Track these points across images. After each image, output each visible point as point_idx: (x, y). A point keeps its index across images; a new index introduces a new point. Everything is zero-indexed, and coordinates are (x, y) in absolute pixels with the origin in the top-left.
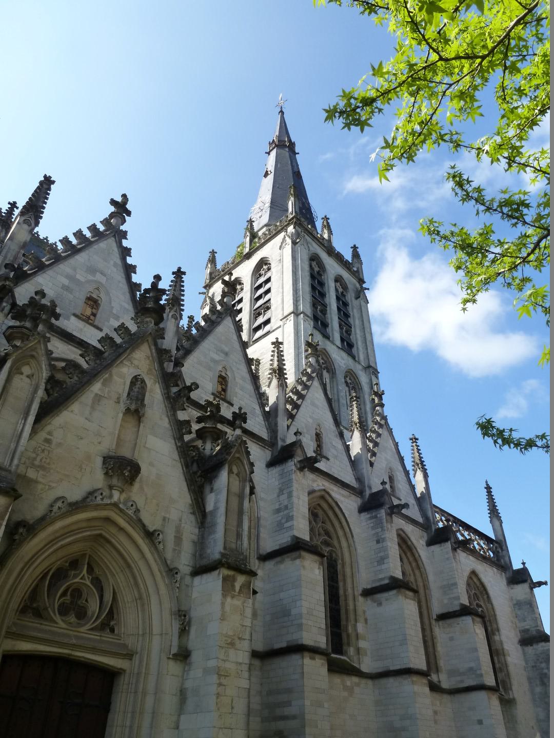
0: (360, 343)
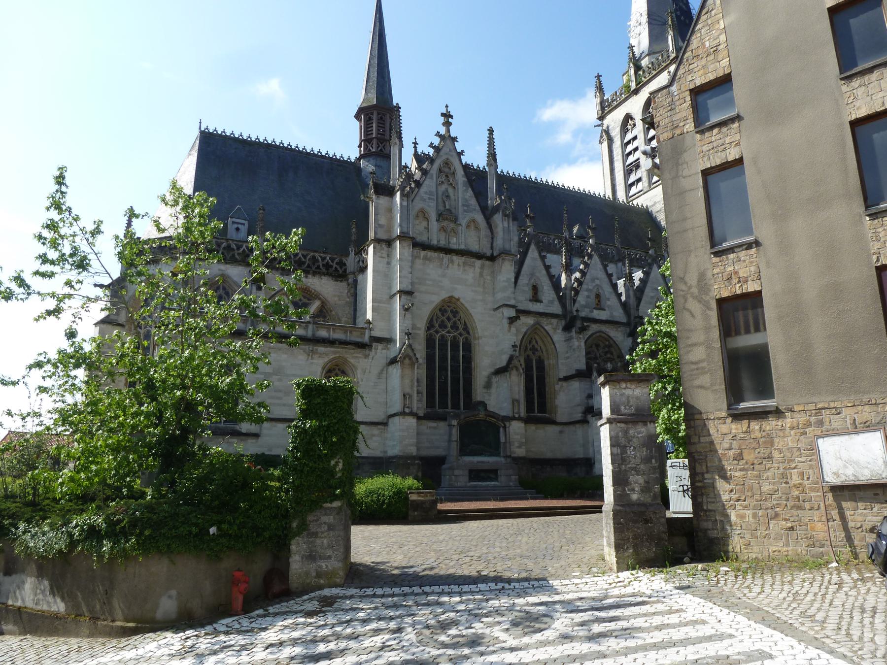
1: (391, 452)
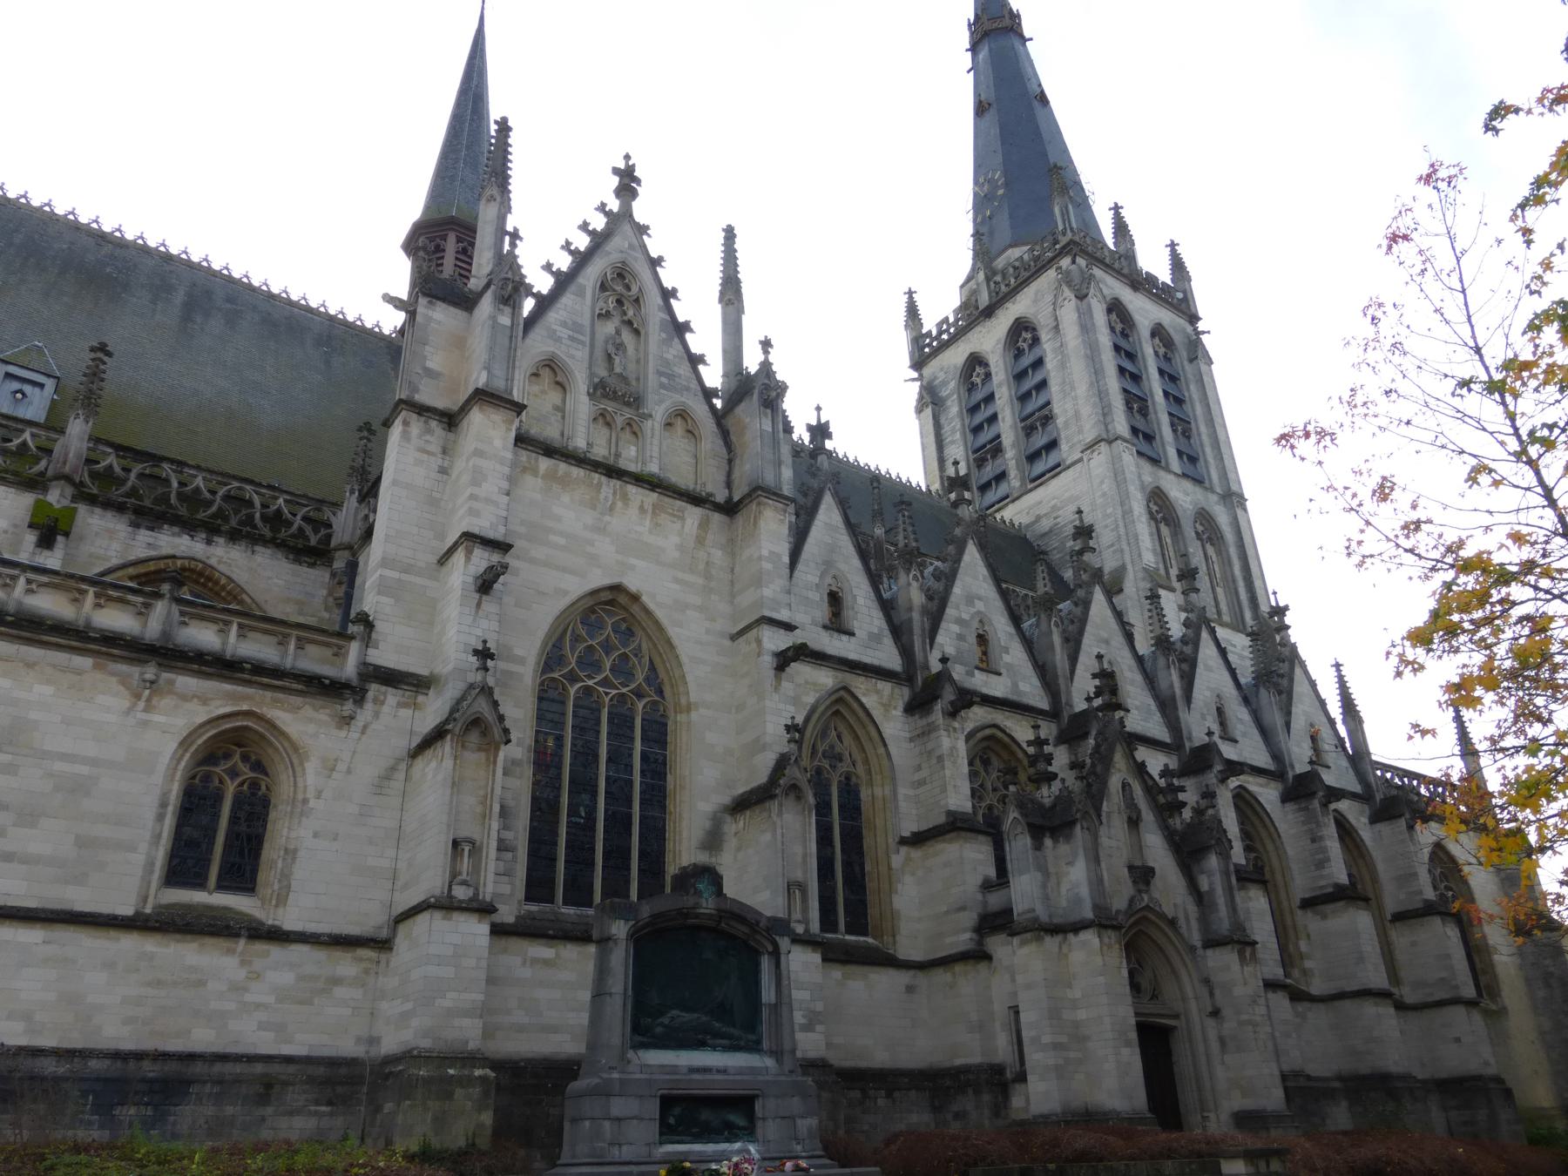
0: (1208, 450)
1: (391, 1042)
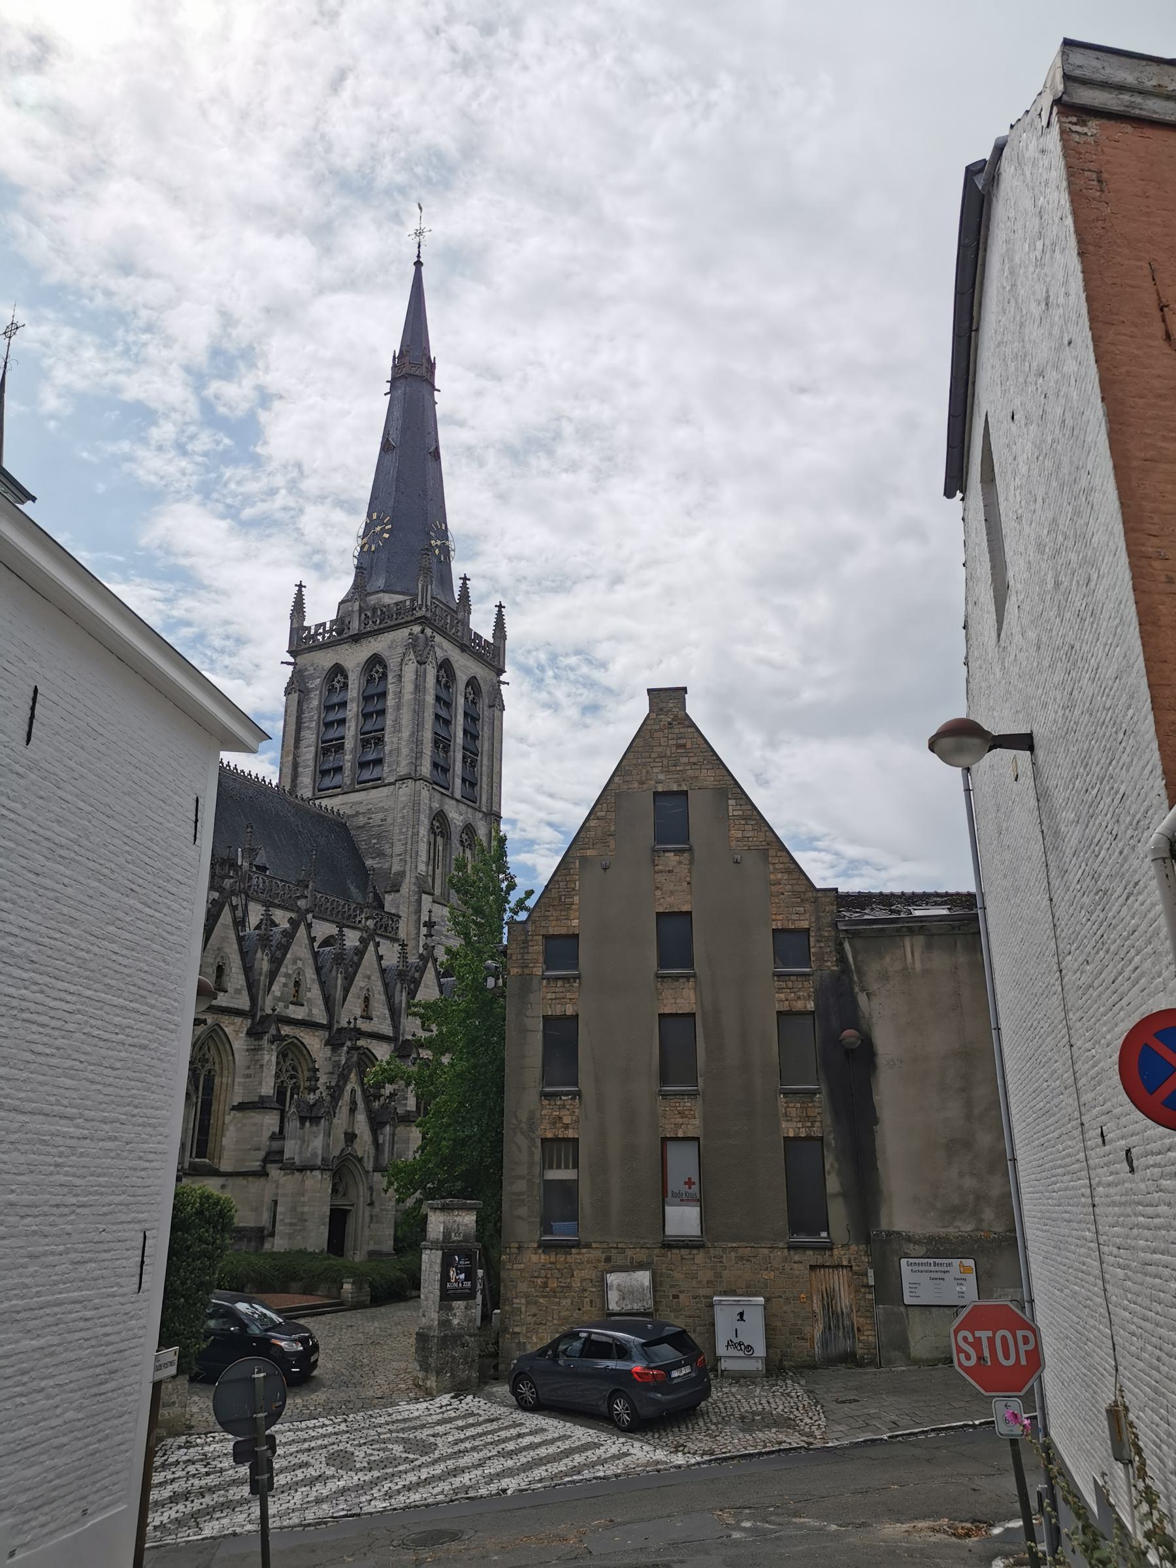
0: (485, 778)
